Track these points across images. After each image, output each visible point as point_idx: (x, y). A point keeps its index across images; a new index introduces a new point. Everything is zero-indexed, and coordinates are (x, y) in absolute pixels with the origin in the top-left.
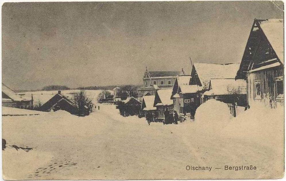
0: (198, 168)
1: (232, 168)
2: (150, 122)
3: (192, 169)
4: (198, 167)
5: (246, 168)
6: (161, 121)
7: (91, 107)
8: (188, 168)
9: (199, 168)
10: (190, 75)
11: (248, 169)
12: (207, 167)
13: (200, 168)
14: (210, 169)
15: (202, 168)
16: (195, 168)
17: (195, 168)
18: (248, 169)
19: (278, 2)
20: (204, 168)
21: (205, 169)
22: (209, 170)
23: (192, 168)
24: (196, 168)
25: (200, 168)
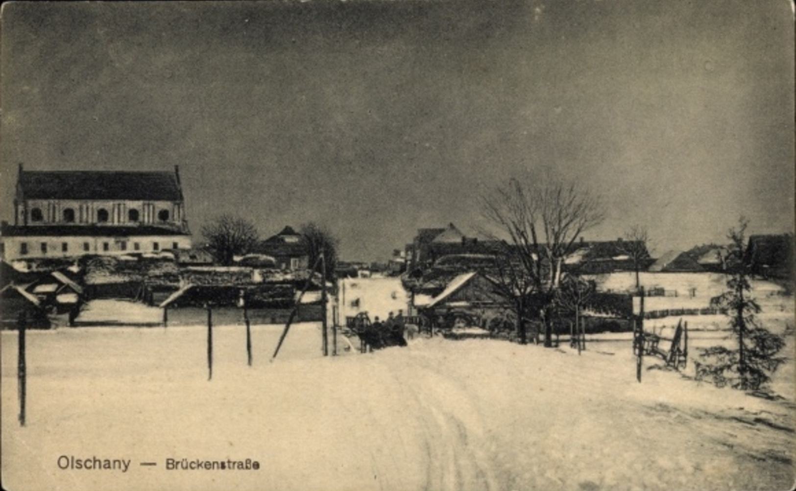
0: (92, 464)
1: (212, 466)
2: (756, 337)
3: (75, 464)
4: (92, 459)
5: (236, 465)
6: (539, 342)
7: (38, 368)
8: (64, 462)
9: (95, 461)
10: (16, 332)
11: (171, 466)
12: (65, 457)
13: (97, 463)
14: (126, 467)
15: (103, 464)
16: (83, 463)
17: (83, 463)
19: (164, 299)
21: (112, 465)
22: (123, 467)
24: (66, 467)
25: (97, 463)
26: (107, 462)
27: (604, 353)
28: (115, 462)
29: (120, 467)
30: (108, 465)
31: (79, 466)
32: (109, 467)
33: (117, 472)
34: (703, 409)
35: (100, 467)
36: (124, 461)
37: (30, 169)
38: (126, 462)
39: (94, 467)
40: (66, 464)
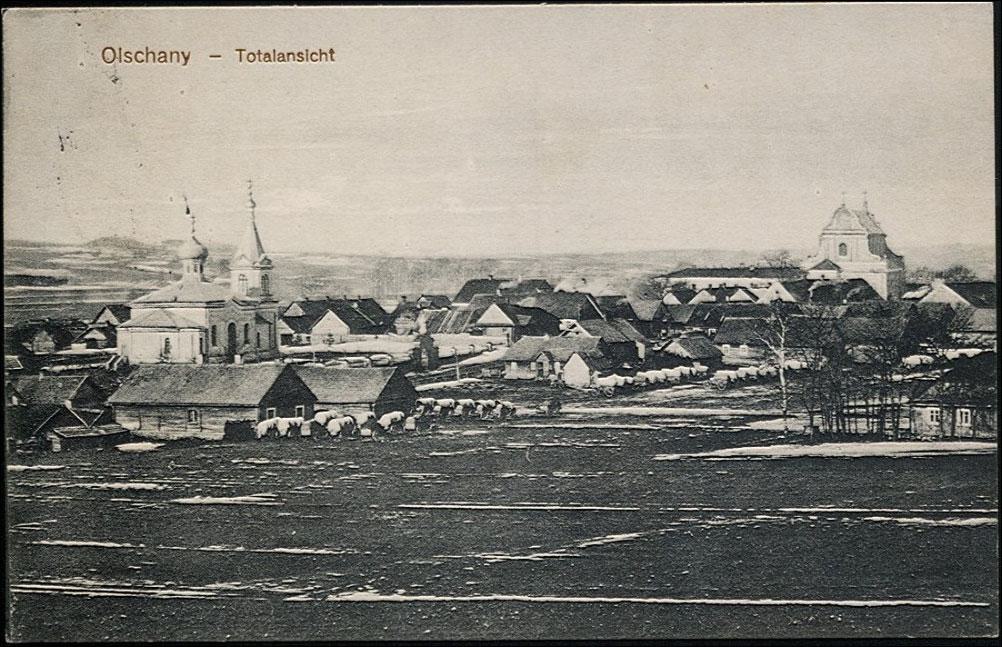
0: (318, 57)
4: (318, 52)
9: (321, 54)
11: (162, 60)
13: (151, 55)
14: (186, 59)
15: (157, 57)
16: (132, 56)
18: (162, 60)
20: (165, 57)
22: (182, 60)
23: (123, 54)
26: (162, 55)
27: (72, 246)
28: (289, 54)
29: (178, 61)
30: (164, 57)
31: (128, 60)
32: (165, 61)
33: (174, 66)
34: (424, 255)
35: (327, 60)
36: (183, 53)
37: (993, 267)
38: (186, 54)
39: (147, 61)
40: (108, 50)
